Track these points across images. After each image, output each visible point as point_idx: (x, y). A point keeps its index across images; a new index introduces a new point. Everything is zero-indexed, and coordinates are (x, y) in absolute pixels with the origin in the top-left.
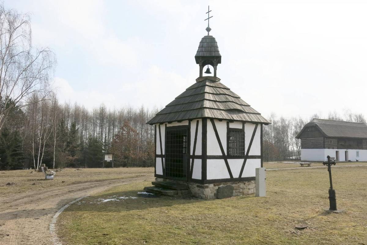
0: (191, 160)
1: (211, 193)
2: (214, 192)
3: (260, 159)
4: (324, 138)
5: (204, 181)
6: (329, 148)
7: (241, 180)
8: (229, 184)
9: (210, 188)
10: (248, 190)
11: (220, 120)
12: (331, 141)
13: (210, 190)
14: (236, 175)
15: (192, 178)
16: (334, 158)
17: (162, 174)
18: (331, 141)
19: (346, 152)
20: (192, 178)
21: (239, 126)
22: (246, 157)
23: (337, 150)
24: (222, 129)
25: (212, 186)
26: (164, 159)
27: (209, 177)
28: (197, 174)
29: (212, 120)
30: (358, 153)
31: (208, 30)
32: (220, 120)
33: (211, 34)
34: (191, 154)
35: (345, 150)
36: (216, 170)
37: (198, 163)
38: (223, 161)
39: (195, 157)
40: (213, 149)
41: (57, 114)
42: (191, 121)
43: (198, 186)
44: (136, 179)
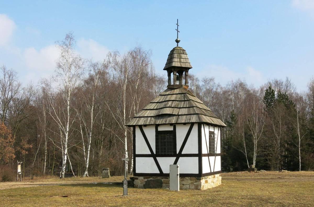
1: (141, 184)
2: (143, 183)
3: (198, 158)
8: (159, 178)
9: (139, 179)
10: (183, 185)
13: (140, 181)
24: (151, 134)
25: (141, 178)
29: (140, 127)
33: (180, 45)
36: (145, 166)
38: (152, 159)
41: (297, 94)
42: (159, 126)
44: (261, 180)
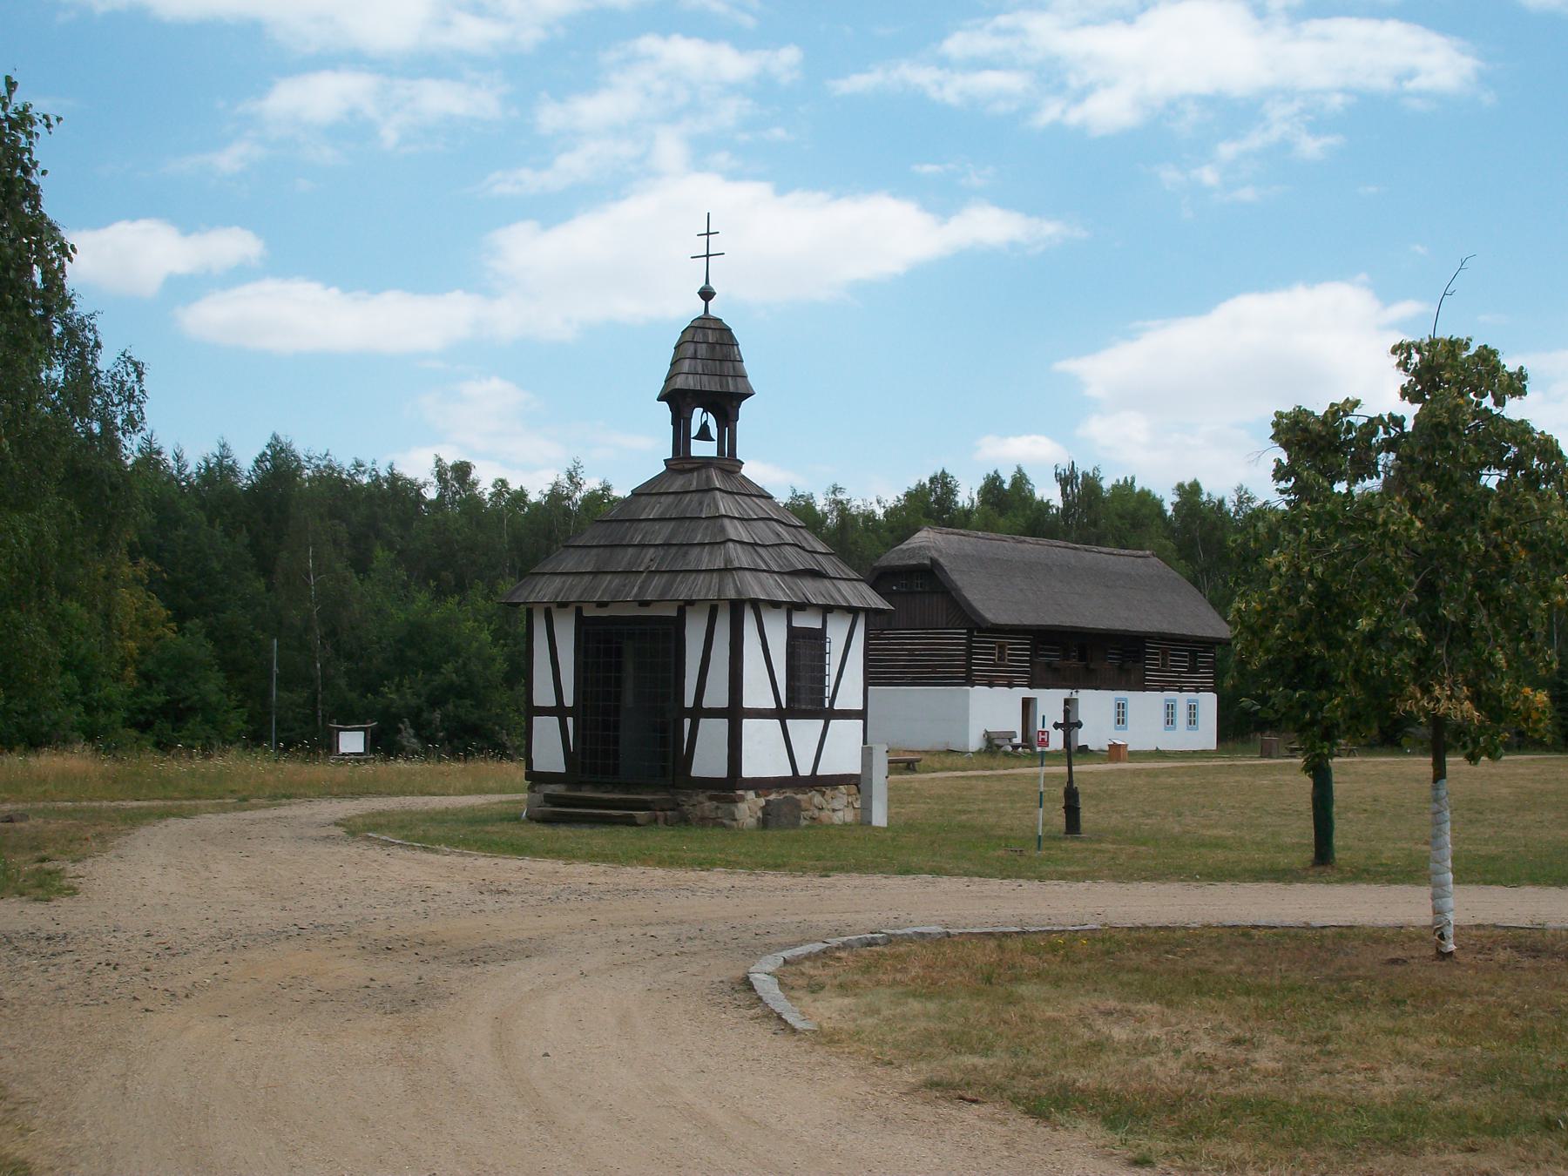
0: (687, 722)
4: (970, 632)
5: (732, 783)
6: (991, 685)
7: (817, 782)
11: (775, 605)
12: (1002, 647)
14: (805, 770)
15: (693, 774)
16: (1013, 734)
17: (559, 767)
18: (1002, 647)
19: (1067, 702)
20: (693, 774)
21: (816, 624)
22: (830, 714)
23: (1027, 692)
26: (570, 721)
27: (748, 771)
28: (708, 760)
29: (756, 604)
30: (1121, 707)
31: (707, 294)
32: (775, 605)
33: (715, 308)
34: (689, 702)
35: (1065, 693)
36: (763, 751)
37: (713, 733)
39: (699, 712)
40: (757, 693)
43: (711, 798)
